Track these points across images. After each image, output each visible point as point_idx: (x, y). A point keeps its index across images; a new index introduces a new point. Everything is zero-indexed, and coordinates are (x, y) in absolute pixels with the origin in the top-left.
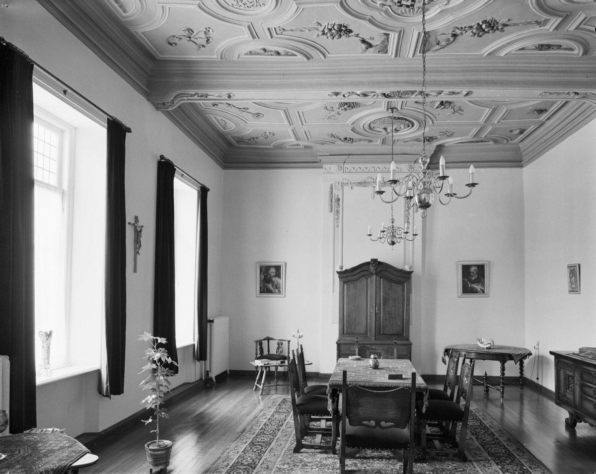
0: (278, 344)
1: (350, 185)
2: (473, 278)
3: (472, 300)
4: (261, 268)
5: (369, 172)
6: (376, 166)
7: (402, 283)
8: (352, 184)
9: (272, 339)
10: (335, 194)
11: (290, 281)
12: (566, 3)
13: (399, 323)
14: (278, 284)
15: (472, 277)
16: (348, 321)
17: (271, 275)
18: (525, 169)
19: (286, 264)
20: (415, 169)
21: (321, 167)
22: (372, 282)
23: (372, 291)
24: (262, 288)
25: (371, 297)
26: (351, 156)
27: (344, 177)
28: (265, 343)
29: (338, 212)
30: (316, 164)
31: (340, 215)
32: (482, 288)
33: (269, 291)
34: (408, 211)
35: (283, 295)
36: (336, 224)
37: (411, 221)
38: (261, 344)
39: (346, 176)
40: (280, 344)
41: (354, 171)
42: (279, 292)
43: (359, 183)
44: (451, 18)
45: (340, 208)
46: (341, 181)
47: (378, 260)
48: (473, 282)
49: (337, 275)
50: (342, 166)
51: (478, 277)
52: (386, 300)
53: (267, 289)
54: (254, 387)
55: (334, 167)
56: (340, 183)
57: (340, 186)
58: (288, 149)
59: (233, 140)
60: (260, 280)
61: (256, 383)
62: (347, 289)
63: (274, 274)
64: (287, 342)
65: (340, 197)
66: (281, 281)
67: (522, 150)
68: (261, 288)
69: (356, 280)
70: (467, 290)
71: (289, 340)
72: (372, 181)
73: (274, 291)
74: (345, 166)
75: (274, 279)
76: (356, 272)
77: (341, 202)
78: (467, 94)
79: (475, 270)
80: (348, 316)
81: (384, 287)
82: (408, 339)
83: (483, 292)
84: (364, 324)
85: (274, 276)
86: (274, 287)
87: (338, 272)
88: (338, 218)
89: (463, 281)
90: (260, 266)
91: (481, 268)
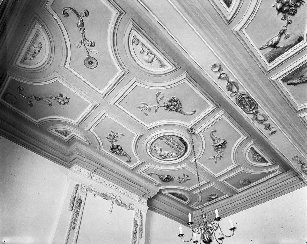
1: (93, 192)
8: (97, 193)
10: (78, 195)
29: (78, 212)
31: (79, 217)
36: (73, 226)
44: (272, 110)
55: (84, 171)
56: (86, 187)
57: (85, 190)
59: (39, 143)
65: (83, 200)
74: (94, 174)
78: (154, 150)
88: (76, 220)
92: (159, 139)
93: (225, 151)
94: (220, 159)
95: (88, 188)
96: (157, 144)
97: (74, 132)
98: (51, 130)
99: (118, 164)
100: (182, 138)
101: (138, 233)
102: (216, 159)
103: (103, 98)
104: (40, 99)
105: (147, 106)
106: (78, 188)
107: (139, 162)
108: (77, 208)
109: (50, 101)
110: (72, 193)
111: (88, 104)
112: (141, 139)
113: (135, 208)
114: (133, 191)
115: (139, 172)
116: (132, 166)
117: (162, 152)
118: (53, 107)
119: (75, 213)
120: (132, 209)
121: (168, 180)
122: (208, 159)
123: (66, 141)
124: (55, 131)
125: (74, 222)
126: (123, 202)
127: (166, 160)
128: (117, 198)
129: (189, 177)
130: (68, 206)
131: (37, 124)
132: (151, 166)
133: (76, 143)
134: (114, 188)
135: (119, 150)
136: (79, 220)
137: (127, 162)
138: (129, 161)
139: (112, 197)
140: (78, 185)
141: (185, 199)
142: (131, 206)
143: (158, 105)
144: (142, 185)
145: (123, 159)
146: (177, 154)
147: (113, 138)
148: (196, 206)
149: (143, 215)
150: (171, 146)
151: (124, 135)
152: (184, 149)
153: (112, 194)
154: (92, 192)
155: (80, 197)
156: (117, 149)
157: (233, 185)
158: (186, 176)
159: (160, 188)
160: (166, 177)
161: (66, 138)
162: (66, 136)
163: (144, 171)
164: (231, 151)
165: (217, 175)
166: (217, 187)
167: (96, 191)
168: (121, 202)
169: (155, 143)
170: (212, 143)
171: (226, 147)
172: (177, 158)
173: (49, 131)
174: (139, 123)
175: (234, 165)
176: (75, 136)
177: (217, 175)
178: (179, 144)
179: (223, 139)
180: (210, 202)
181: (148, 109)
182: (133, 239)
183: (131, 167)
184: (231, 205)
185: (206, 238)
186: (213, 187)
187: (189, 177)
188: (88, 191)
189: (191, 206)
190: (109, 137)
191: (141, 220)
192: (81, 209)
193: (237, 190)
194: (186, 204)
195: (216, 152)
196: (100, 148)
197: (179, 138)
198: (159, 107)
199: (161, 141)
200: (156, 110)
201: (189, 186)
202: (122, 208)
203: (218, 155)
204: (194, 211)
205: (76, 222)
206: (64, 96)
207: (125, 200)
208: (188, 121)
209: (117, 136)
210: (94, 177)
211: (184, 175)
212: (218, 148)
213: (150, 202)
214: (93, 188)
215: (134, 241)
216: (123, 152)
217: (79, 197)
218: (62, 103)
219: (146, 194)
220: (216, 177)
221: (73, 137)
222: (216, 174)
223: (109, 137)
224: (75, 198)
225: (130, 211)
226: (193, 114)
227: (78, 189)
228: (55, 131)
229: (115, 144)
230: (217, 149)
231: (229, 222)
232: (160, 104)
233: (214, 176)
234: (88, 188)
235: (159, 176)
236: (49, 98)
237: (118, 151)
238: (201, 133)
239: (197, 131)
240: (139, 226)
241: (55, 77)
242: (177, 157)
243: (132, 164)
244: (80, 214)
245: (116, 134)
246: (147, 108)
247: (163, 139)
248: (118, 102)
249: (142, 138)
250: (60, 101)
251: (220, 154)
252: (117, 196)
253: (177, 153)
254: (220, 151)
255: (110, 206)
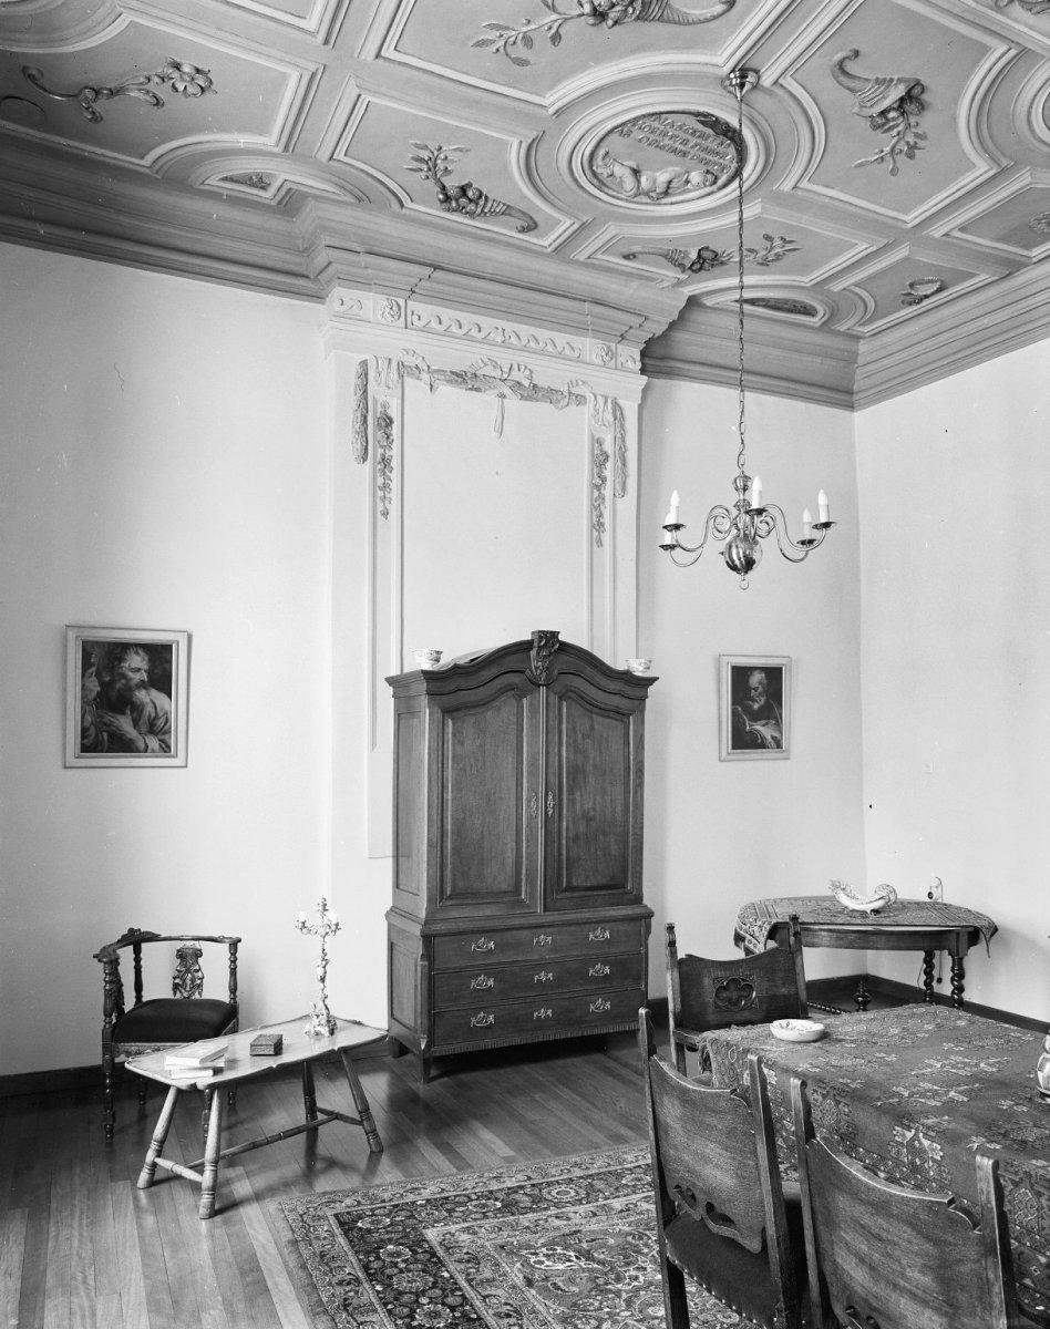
0: (181, 955)
1: (425, 376)
2: (756, 706)
3: (754, 764)
4: (89, 649)
5: (485, 341)
6: (510, 326)
7: (621, 715)
9: (153, 938)
10: (375, 401)
11: (205, 701)
12: (974, 5)
13: (614, 850)
14: (157, 717)
15: (754, 700)
16: (456, 851)
17: (129, 680)
18: (860, 417)
19: (190, 637)
20: (620, 359)
21: (318, 297)
22: (534, 711)
23: (533, 744)
24: (92, 730)
25: (533, 764)
26: (439, 274)
27: (408, 346)
28: (126, 954)
30: (301, 282)
31: (395, 475)
32: (776, 734)
33: (121, 745)
34: (598, 488)
35: (179, 761)
36: (380, 507)
37: (607, 520)
38: (113, 964)
39: (413, 340)
40: (188, 959)
41: (440, 328)
42: (165, 748)
43: (457, 375)
45: (395, 452)
46: (397, 356)
47: (561, 638)
48: (755, 717)
49: (387, 695)
50: (402, 302)
51: (767, 701)
52: (577, 774)
53: (110, 735)
54: (144, 1176)
55: (373, 303)
56: (394, 365)
58: (214, 196)
60: (83, 697)
61: (150, 1156)
62: (454, 735)
63: (145, 677)
64: (225, 947)
65: (394, 413)
66: (175, 706)
67: (861, 361)
68: (84, 731)
69: (485, 703)
70: (743, 740)
71: (235, 936)
72: (497, 374)
73: (142, 746)
75: (142, 696)
76: (486, 674)
77: (395, 430)
79: (760, 683)
80: (459, 832)
81: (572, 730)
82: (638, 899)
83: (779, 746)
84: (510, 856)
85: (142, 685)
86: (144, 728)
87: (391, 681)
88: (385, 487)
89: (734, 713)
90: (85, 643)
91: (774, 675)
92: (615, 137)
93: (927, 122)
94: (911, 156)
95: (401, 365)
96: (612, 154)
97: (284, 174)
98: (206, 182)
99: (492, 241)
100: (707, 115)
101: (609, 483)
102: (889, 159)
103: (326, 42)
104: (112, 93)
105: (514, 33)
106: (366, 375)
107: (566, 225)
108: (382, 447)
109: (148, 92)
110: (352, 401)
111: (284, 77)
112: (540, 149)
113: (590, 396)
114: (580, 329)
115: (582, 258)
116: (547, 241)
117: (643, 179)
118: (167, 106)
119: (379, 466)
120: (580, 400)
121: (707, 261)
122: (856, 166)
123: (273, 203)
124: (219, 180)
125: (380, 493)
126: (539, 385)
127: (672, 204)
128: (516, 375)
129: (790, 242)
130: (351, 447)
131: (147, 171)
132: (618, 231)
133: (311, 203)
134: (499, 339)
135: (471, 201)
136: (395, 485)
137: (523, 230)
138: (531, 226)
139: (493, 375)
140: (364, 364)
141: (808, 311)
142: (573, 390)
143: (555, 16)
144: (612, 298)
145: (505, 225)
146: (709, 176)
147: (431, 166)
148: (863, 324)
149: (626, 413)
150: (674, 151)
151: (468, 147)
152: (732, 152)
153: (495, 365)
154: (418, 378)
155: (384, 406)
156: (463, 201)
157: (999, 240)
158: (778, 242)
159: (689, 291)
160: (694, 256)
161: (267, 195)
162: (264, 188)
163: (606, 248)
164: (954, 118)
165: (912, 216)
166: (926, 257)
167: (433, 367)
168: (535, 386)
169: (601, 152)
170: (853, 106)
171: (922, 107)
172: (714, 188)
173: (202, 187)
174: (505, 100)
175: (982, 169)
176: (295, 187)
177: (911, 218)
178: (703, 136)
179: (900, 80)
180: (919, 306)
181: (519, 41)
182: (592, 504)
183: (546, 244)
184: (1006, 312)
185: (735, 557)
186: (907, 259)
187: (790, 242)
188: (405, 378)
189: (843, 328)
190: (415, 165)
191: (619, 435)
192: (394, 446)
193: (1025, 253)
194: (818, 325)
195: (885, 132)
196: (402, 206)
197: (697, 114)
198: (560, 21)
199: (626, 140)
200: (556, 38)
201: (805, 269)
202: (542, 408)
203: (897, 143)
204: (862, 341)
205: (387, 495)
206: (186, 69)
207: (549, 373)
208: (714, 43)
209: (442, 156)
210: (415, 317)
211: (768, 238)
212: (888, 120)
213: (657, 359)
214: (419, 362)
215: (595, 513)
216: (489, 205)
217: (380, 409)
218: (190, 90)
219: (631, 328)
220: (910, 226)
221: (290, 189)
222: (906, 212)
223: (415, 165)
224: (365, 417)
225: (573, 407)
226: (725, 12)
227: (367, 380)
228: (219, 180)
229: (452, 183)
230: (884, 125)
231: (802, 519)
232: (561, 10)
233: (900, 224)
234: (401, 365)
235: (665, 256)
236: (141, 84)
237: (472, 207)
238: (789, 79)
239: (769, 73)
240: (611, 460)
241: (117, 13)
242: (715, 182)
243: (546, 234)
244: (395, 463)
245: (436, 153)
246: (513, 39)
247: (629, 133)
248: (389, 45)
249: (543, 148)
250: (181, 88)
251: (907, 139)
252: (516, 367)
253: (708, 172)
254: (900, 128)
255: (496, 412)
